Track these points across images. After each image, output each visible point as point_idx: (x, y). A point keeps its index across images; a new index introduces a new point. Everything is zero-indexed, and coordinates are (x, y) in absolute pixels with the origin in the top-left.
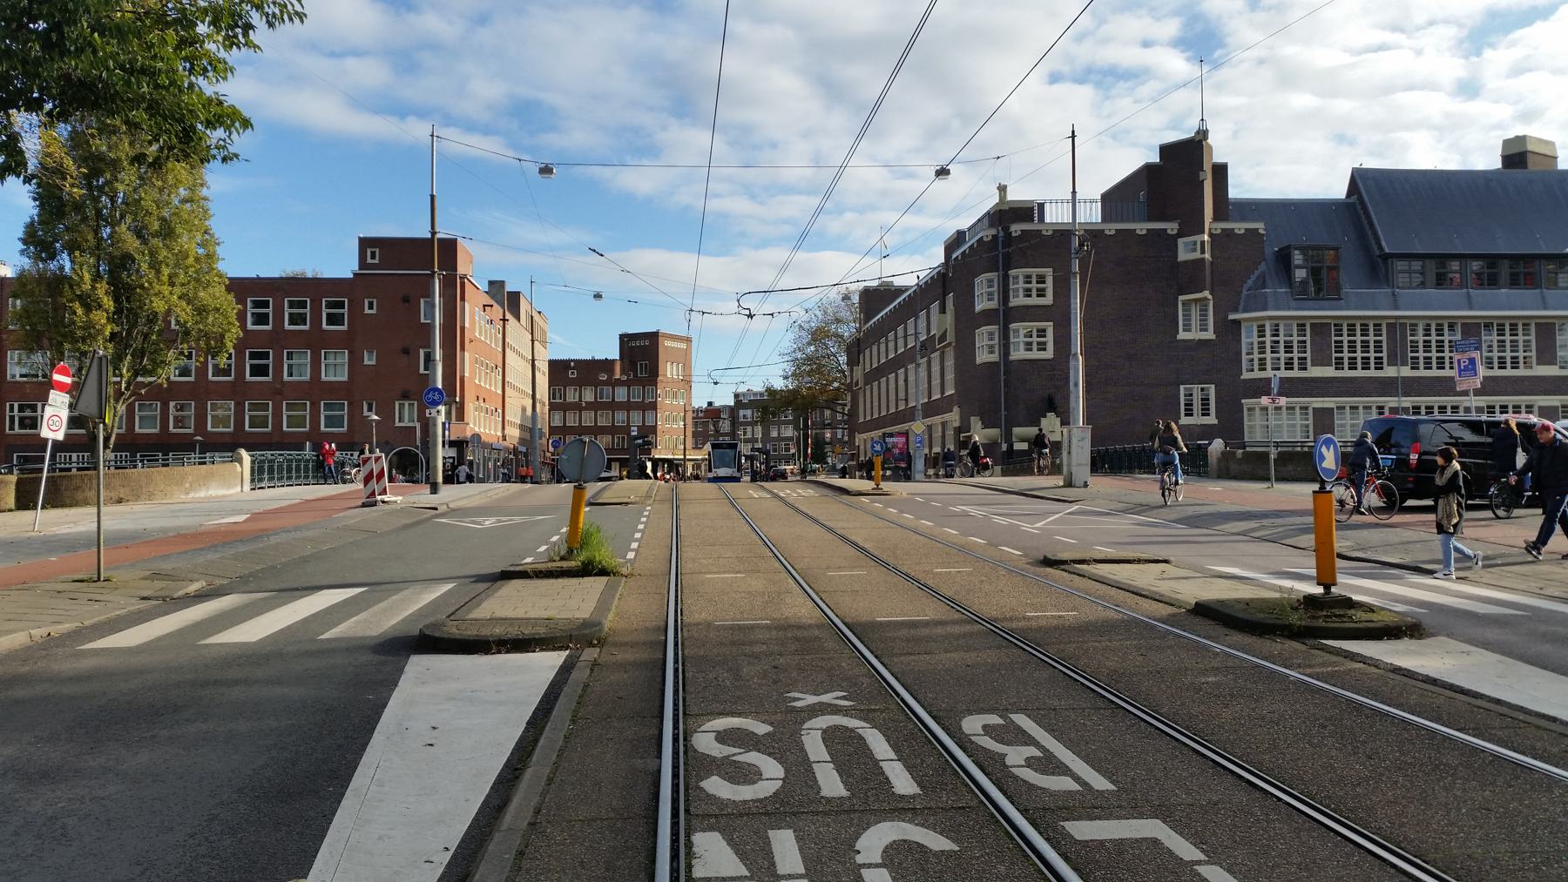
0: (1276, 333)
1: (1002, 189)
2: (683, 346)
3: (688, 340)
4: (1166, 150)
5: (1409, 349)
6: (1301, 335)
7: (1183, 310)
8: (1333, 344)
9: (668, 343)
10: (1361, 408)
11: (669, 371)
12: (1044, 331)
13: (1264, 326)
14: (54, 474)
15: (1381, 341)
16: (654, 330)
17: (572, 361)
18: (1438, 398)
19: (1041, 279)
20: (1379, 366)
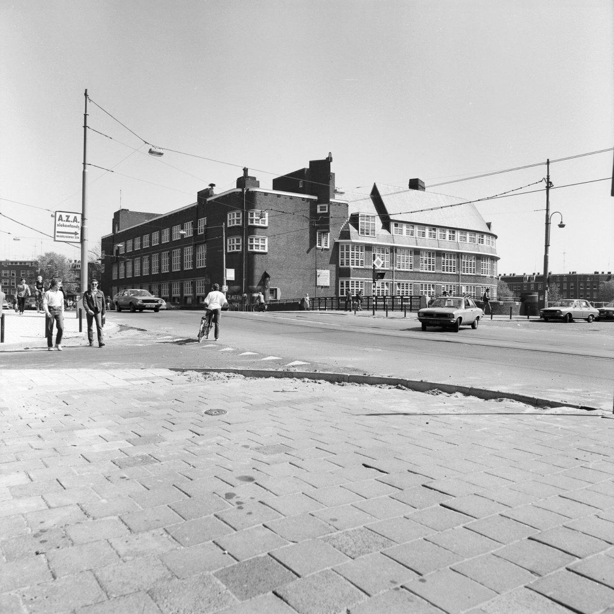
0: (348, 249)
1: (245, 170)
12: (264, 240)
13: (349, 246)
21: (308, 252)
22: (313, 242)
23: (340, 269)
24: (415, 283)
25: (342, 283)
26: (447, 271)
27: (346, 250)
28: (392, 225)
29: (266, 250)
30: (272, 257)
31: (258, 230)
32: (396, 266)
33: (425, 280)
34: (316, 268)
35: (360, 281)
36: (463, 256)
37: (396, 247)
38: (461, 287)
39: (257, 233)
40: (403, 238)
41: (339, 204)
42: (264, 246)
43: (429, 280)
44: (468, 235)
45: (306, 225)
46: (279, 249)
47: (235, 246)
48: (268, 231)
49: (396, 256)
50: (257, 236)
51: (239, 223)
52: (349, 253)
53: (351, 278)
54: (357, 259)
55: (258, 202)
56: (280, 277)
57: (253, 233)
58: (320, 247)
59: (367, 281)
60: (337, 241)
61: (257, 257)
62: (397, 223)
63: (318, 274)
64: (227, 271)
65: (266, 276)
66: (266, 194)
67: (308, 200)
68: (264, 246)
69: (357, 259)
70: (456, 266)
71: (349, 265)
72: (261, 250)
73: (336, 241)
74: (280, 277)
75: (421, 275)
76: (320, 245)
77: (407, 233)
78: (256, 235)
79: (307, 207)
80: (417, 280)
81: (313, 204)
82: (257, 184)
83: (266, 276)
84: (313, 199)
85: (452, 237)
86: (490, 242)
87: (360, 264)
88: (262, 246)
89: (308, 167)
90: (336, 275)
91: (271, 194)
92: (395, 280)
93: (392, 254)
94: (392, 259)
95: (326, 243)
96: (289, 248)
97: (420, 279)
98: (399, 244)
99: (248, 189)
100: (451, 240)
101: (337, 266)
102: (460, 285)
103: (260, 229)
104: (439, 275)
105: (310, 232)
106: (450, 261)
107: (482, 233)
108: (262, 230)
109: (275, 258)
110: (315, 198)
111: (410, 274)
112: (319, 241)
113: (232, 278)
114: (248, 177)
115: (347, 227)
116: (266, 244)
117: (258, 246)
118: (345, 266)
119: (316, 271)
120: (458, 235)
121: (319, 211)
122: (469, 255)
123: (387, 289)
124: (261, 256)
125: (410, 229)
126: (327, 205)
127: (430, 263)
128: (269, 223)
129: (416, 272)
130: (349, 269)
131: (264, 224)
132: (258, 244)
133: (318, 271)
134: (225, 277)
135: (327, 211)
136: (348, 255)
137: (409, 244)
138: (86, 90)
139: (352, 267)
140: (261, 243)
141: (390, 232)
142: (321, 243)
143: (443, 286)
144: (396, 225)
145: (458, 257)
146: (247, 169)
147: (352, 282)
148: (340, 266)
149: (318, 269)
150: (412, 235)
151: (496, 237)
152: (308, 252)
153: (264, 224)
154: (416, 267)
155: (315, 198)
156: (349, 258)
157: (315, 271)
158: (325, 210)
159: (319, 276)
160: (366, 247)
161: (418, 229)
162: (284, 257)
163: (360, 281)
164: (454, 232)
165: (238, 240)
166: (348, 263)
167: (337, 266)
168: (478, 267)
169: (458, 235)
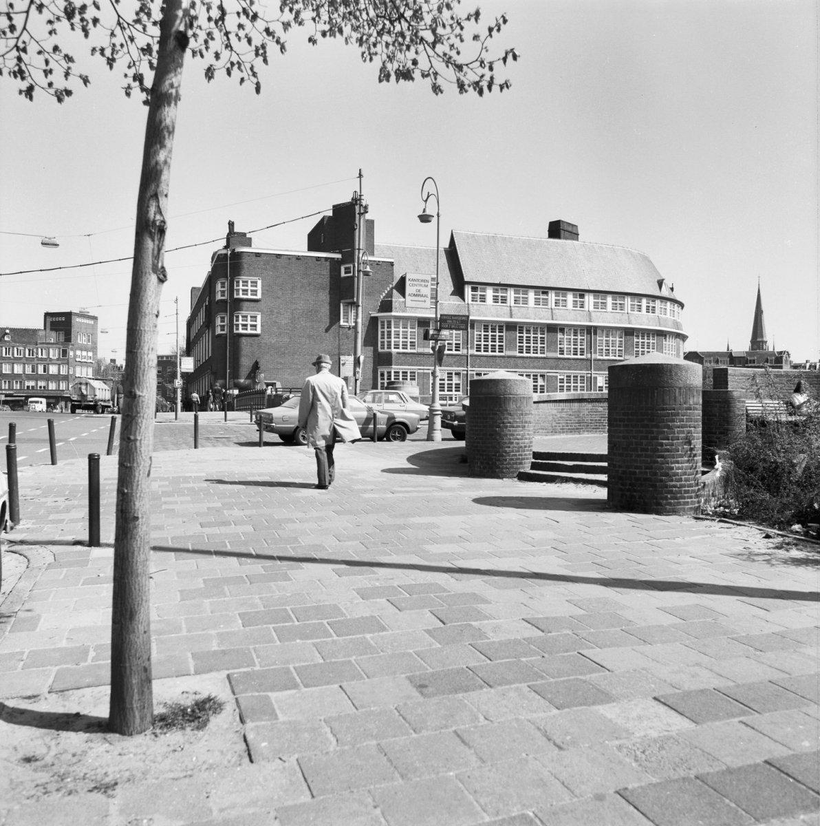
0: (389, 327)
1: (231, 224)
2: (92, 322)
3: (95, 318)
4: (337, 208)
5: (518, 341)
6: (405, 328)
7: (344, 312)
8: (518, 338)
9: (78, 320)
10: (401, 373)
11: (80, 339)
12: (256, 317)
13: (390, 321)
14: (583, 392)
15: (502, 336)
16: (69, 311)
17: (7, 328)
18: (402, 367)
19: (254, 283)
20: (501, 350)
21: (327, 330)
22: (335, 317)
23: (380, 354)
24: (548, 374)
25: (382, 375)
26: (486, 351)
27: (388, 328)
28: (468, 290)
29: (259, 331)
30: (262, 336)
31: (246, 304)
32: (595, 353)
33: (526, 368)
34: (339, 354)
35: (409, 372)
36: (598, 331)
37: (596, 328)
38: (596, 378)
39: (244, 308)
40: (486, 310)
41: (258, 255)
42: (255, 326)
43: (534, 368)
44: (609, 299)
45: (325, 297)
46: (279, 328)
47: (240, 326)
48: (262, 305)
49: (596, 340)
50: (244, 313)
51: (224, 296)
52: (390, 332)
53: (393, 366)
54: (486, 343)
55: (245, 266)
56: (279, 366)
57: (239, 309)
58: (346, 324)
59: (422, 371)
60: (375, 314)
61: (244, 340)
62: (475, 286)
63: (342, 362)
64: (182, 361)
65: (256, 367)
66: (298, 258)
67: (326, 259)
68: (255, 326)
69: (486, 343)
70: (585, 347)
71: (390, 348)
72: (249, 331)
73: (372, 315)
74: (279, 366)
75: (520, 361)
76: (347, 322)
77: (496, 300)
78: (242, 310)
79: (326, 271)
80: (512, 368)
81: (335, 265)
82: (248, 242)
83: (256, 367)
84: (334, 258)
85: (618, 306)
86: (676, 312)
87: (579, 353)
88: (251, 326)
89: (330, 213)
90: (374, 363)
91: (270, 254)
92: (469, 369)
93: (589, 336)
94: (465, 338)
95: (354, 319)
96: (296, 328)
97: (563, 368)
98: (479, 316)
99: (234, 250)
100: (500, 304)
101: (376, 350)
102: (593, 376)
103: (249, 303)
104: (552, 361)
105: (331, 304)
106: (606, 341)
107: (653, 298)
108: (252, 304)
109: (273, 342)
110: (339, 256)
111: (498, 360)
112: (344, 316)
113: (189, 369)
114: (235, 233)
115: (390, 295)
116: (259, 323)
117: (246, 325)
118: (386, 350)
119: (339, 359)
120: (589, 300)
121: (343, 274)
122: (609, 330)
123: (458, 382)
124: (249, 339)
125: (618, 302)
126: (352, 266)
127: (643, 348)
128: (263, 294)
129: (509, 357)
130: (390, 354)
131: (256, 295)
132: (246, 323)
133: (342, 358)
134: (178, 369)
135: (351, 274)
136: (389, 334)
137: (498, 317)
138: (360, 170)
139: (394, 351)
140: (251, 321)
141: (464, 300)
142: (347, 318)
143: (562, 377)
144: (474, 289)
145: (589, 333)
146: (233, 223)
147: (395, 372)
148: (380, 350)
149: (344, 355)
150: (583, 307)
151: (682, 305)
152: (327, 330)
153: (256, 295)
154: (509, 350)
155: (339, 256)
156: (390, 338)
157: (337, 357)
158: (350, 272)
159: (344, 364)
160: (506, 326)
161: (631, 301)
162: (286, 340)
163: (409, 372)
164: (582, 296)
165: (223, 319)
166: (389, 347)
167: (376, 350)
168: (552, 345)
169: (589, 300)
